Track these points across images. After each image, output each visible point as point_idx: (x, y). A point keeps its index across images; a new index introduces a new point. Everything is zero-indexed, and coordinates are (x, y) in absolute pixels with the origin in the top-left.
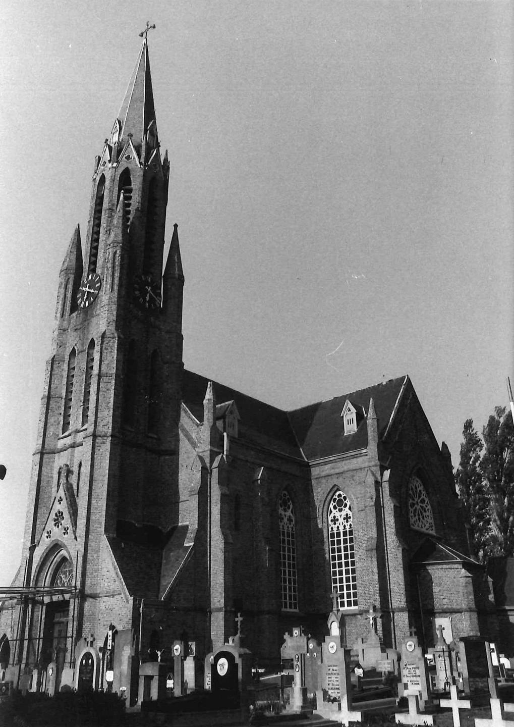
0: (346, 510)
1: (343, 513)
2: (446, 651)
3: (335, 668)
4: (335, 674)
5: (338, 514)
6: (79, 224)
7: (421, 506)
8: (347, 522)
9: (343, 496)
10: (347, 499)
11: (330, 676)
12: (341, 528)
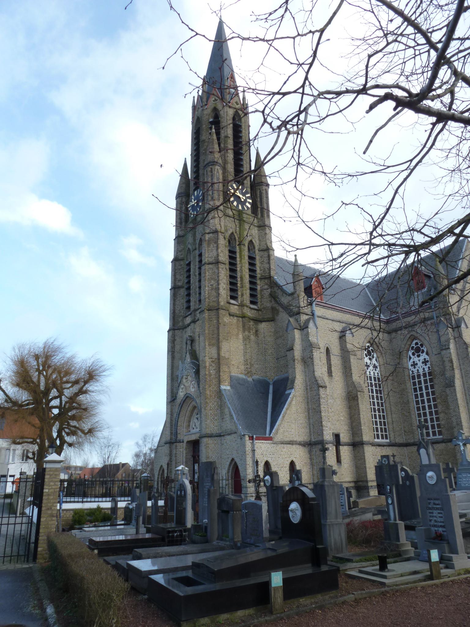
0: (424, 356)
3: (437, 502)
4: (437, 509)
5: (416, 359)
9: (419, 344)
11: (431, 511)
12: (421, 371)
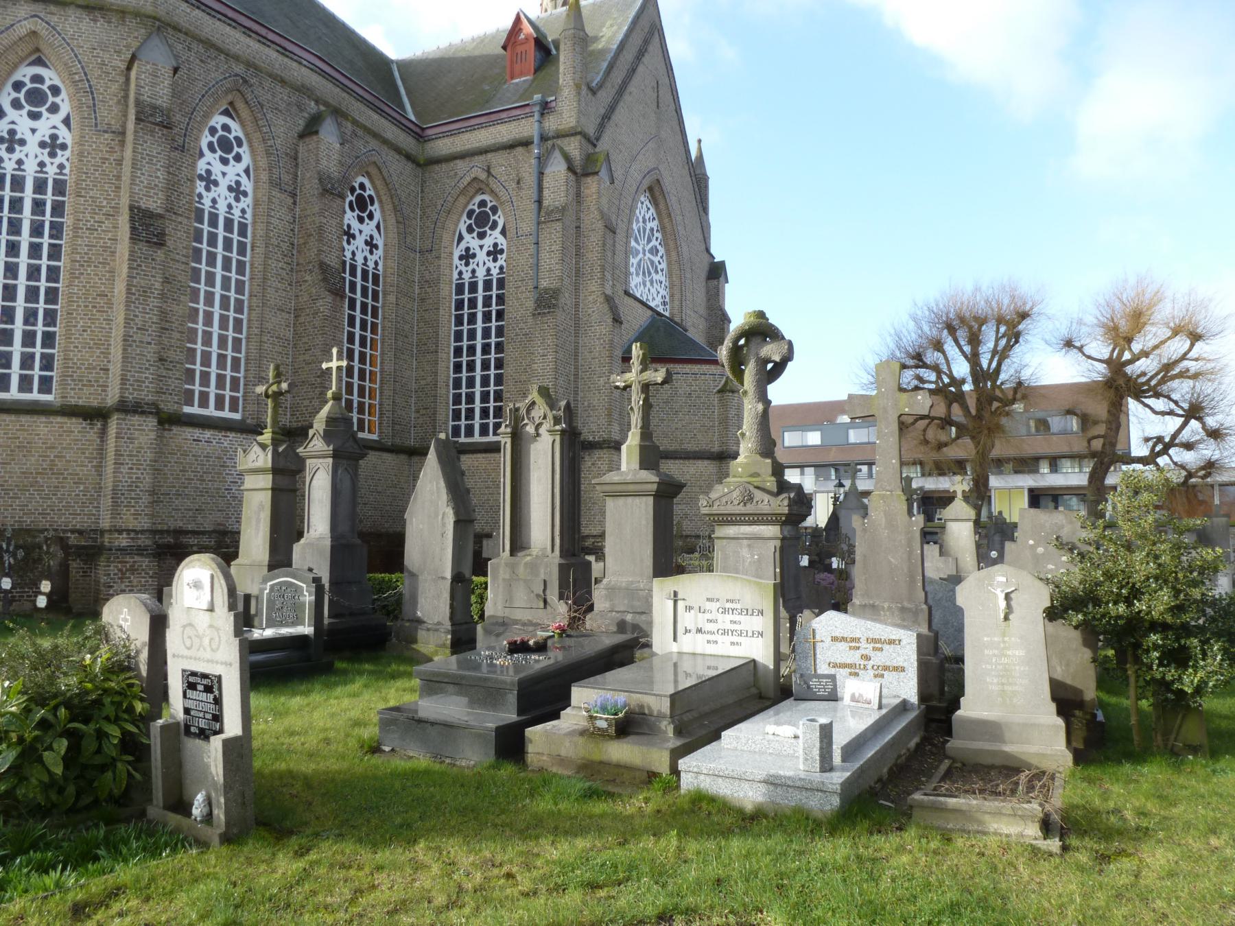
0: (494, 237)
1: (488, 242)
8: (495, 260)
9: (489, 205)
10: (500, 212)
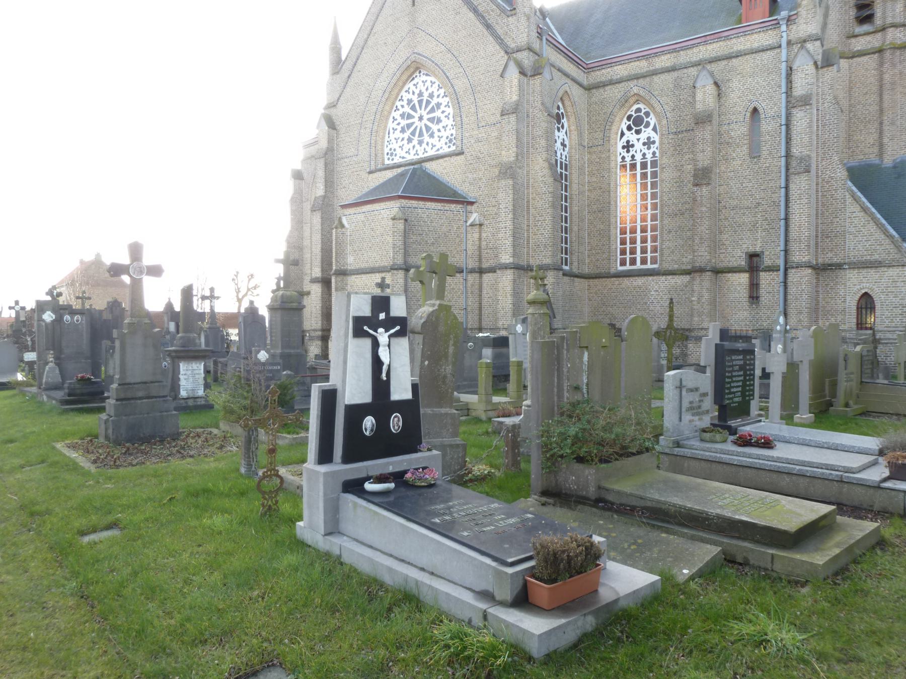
1: (643, 136)
2: (83, 304)
6: (681, 380)
7: (415, 111)
9: (643, 111)
10: (652, 115)
12: (638, 157)
